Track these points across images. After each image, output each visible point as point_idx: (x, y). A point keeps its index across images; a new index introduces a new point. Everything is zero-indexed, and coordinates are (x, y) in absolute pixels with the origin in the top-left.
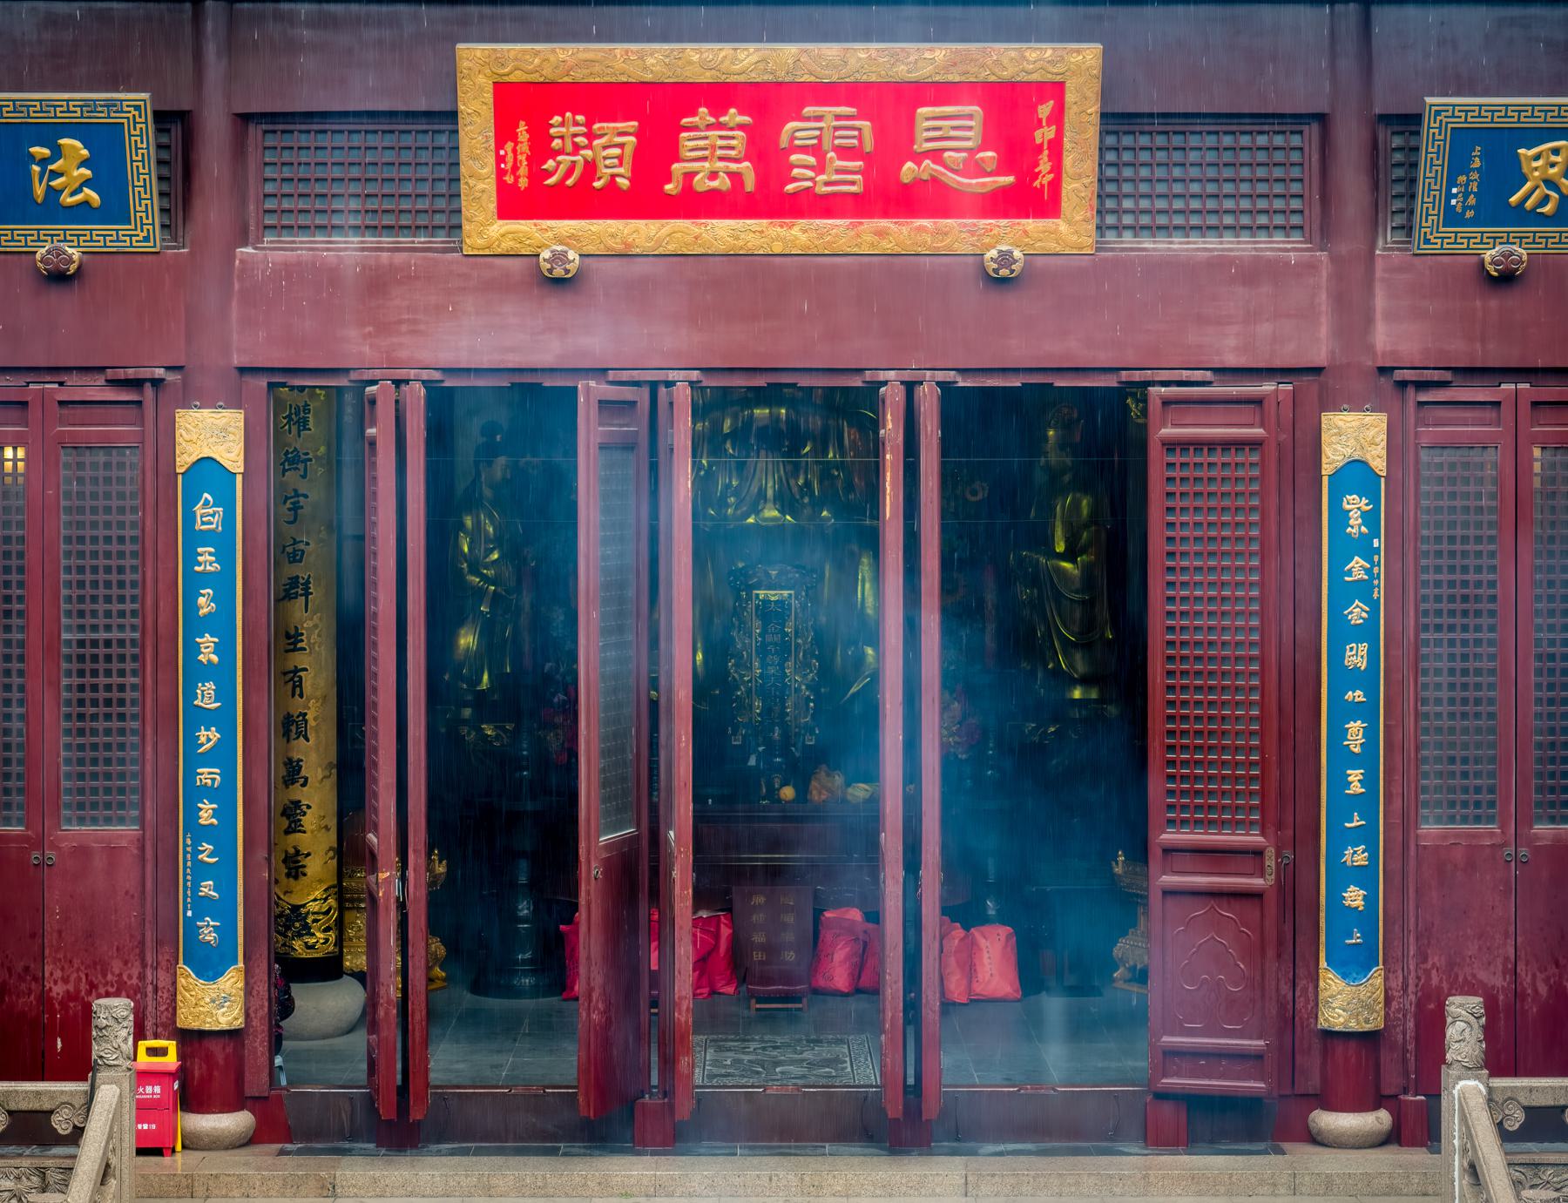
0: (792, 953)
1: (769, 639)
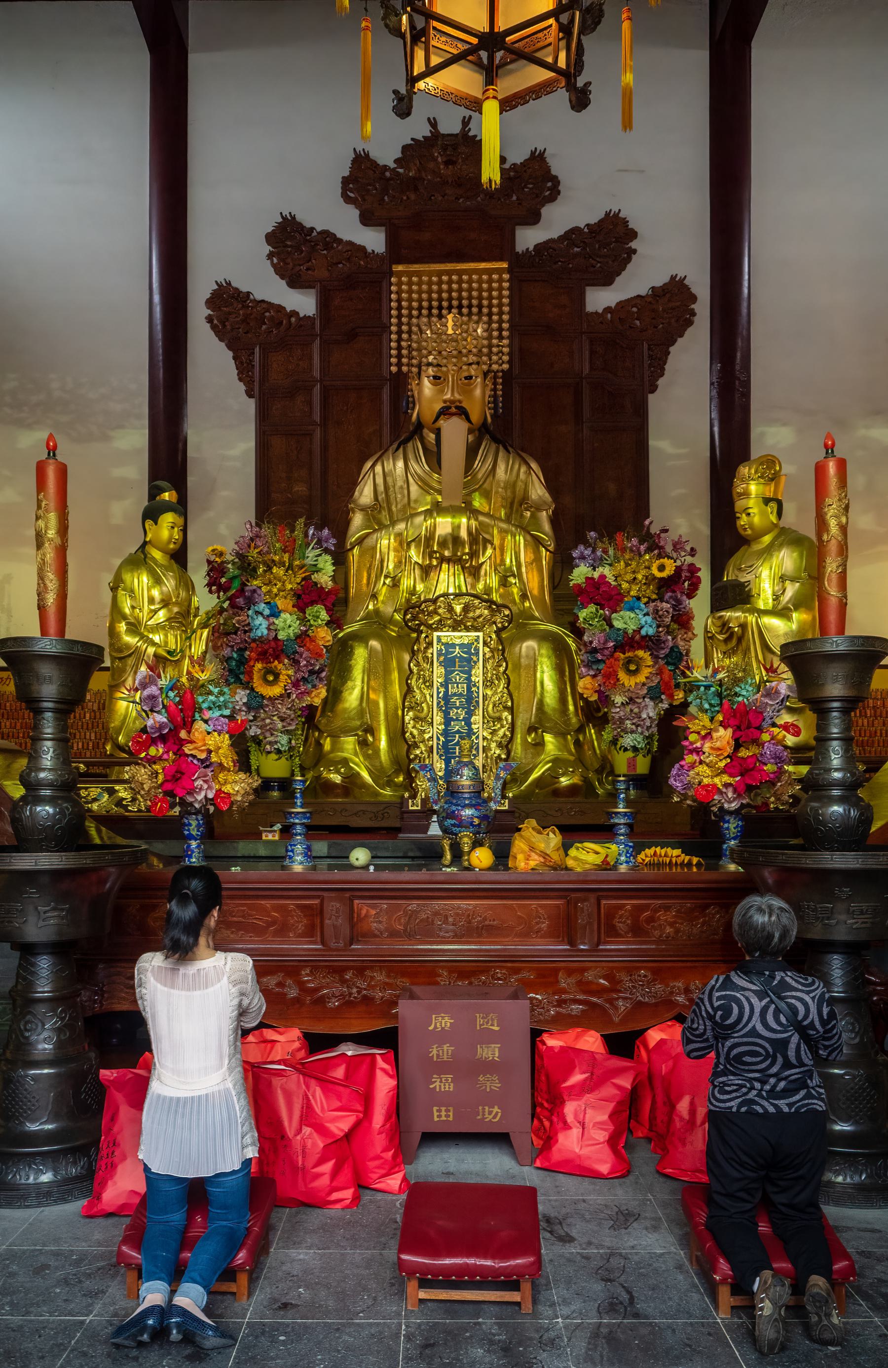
0: (496, 1109)
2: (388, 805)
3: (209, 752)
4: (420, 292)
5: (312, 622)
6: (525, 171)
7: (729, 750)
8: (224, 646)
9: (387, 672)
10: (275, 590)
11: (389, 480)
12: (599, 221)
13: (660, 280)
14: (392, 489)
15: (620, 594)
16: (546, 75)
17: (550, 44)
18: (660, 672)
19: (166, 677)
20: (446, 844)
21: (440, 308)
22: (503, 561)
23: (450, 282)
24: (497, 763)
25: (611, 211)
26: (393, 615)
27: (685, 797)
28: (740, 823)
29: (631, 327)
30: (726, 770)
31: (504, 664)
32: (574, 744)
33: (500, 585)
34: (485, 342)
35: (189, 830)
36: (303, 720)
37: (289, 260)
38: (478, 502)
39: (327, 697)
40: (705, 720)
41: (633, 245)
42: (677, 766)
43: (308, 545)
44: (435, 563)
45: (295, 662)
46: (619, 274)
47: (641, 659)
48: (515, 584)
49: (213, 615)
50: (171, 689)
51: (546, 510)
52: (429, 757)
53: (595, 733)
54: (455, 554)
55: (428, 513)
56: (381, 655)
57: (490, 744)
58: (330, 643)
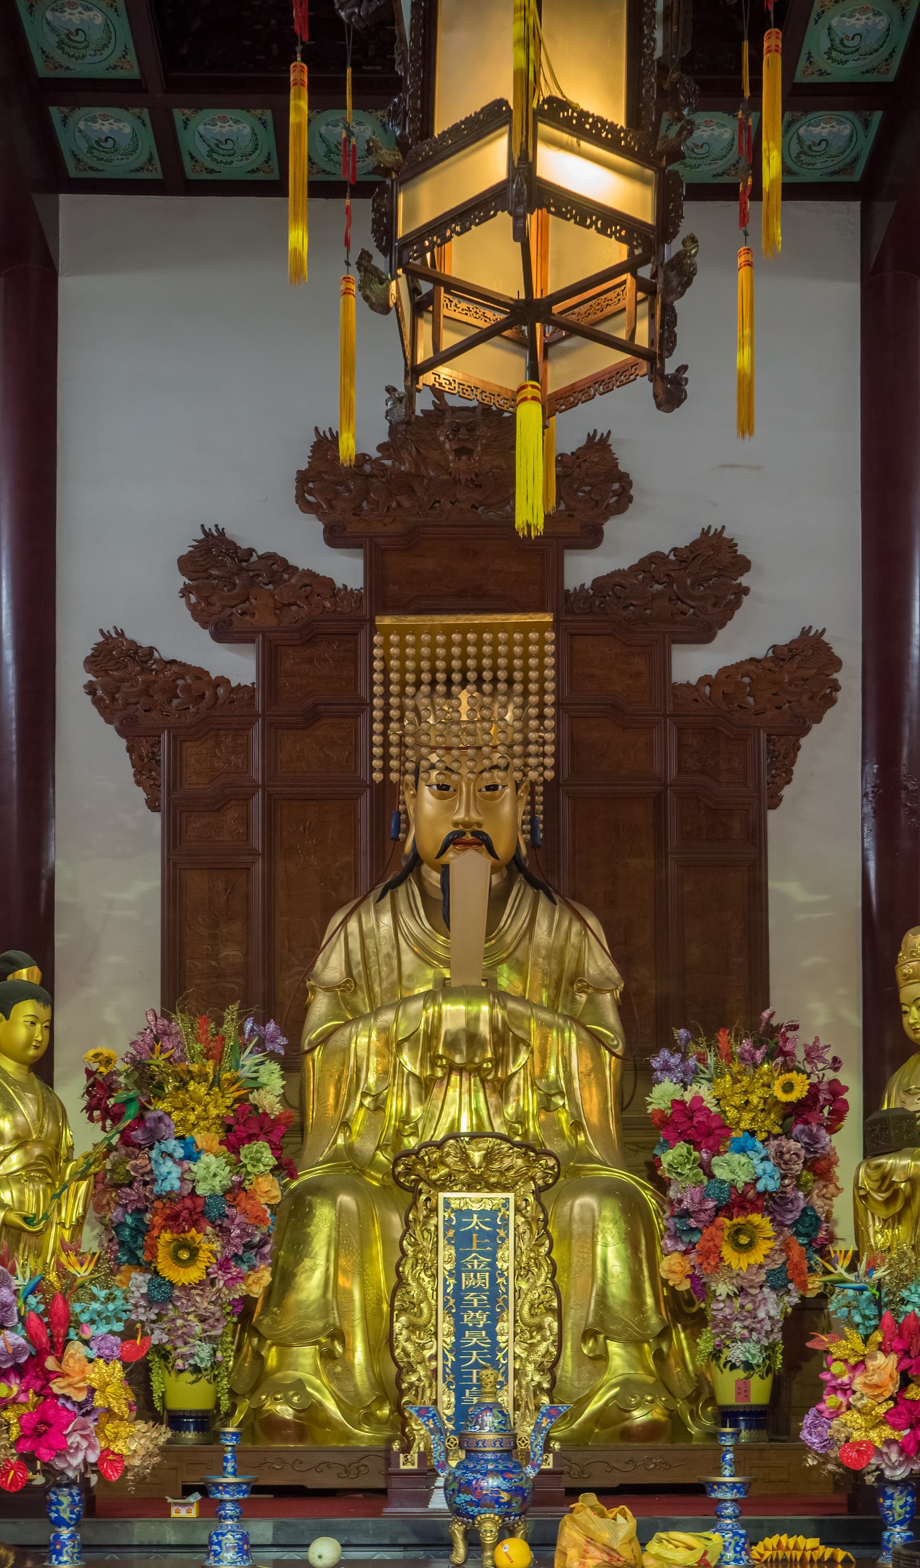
1: (467, 1281)
2: (367, 1453)
3: (92, 1391)
4: (418, 658)
5: (249, 1168)
6: (579, 466)
7: (892, 1388)
8: (112, 1205)
9: (365, 1242)
10: (192, 1118)
11: (370, 943)
13: (786, 635)
14: (373, 958)
15: (724, 1127)
16: (617, 357)
17: (624, 310)
18: (786, 1248)
19: (24, 1273)
20: (458, 1531)
21: (449, 682)
22: (544, 1071)
23: (464, 644)
24: (535, 1395)
26: (374, 1155)
27: (826, 1459)
28: (909, 1499)
29: (741, 707)
30: (889, 1419)
31: (547, 1242)
32: (654, 1356)
33: (539, 1109)
34: (518, 737)
35: (57, 1511)
36: (235, 1319)
37: (214, 599)
38: (506, 979)
39: (271, 1285)
40: (855, 1340)
41: (744, 580)
42: (813, 1411)
43: (243, 1047)
44: (439, 1073)
45: (224, 1231)
46: (722, 625)
47: (756, 1227)
48: (564, 1106)
49: (95, 1160)
50: (32, 1292)
51: (611, 991)
52: (430, 1386)
53: (686, 1337)
54: (470, 1060)
55: (430, 997)
56: (356, 1217)
57: (524, 1366)
58: (278, 1201)
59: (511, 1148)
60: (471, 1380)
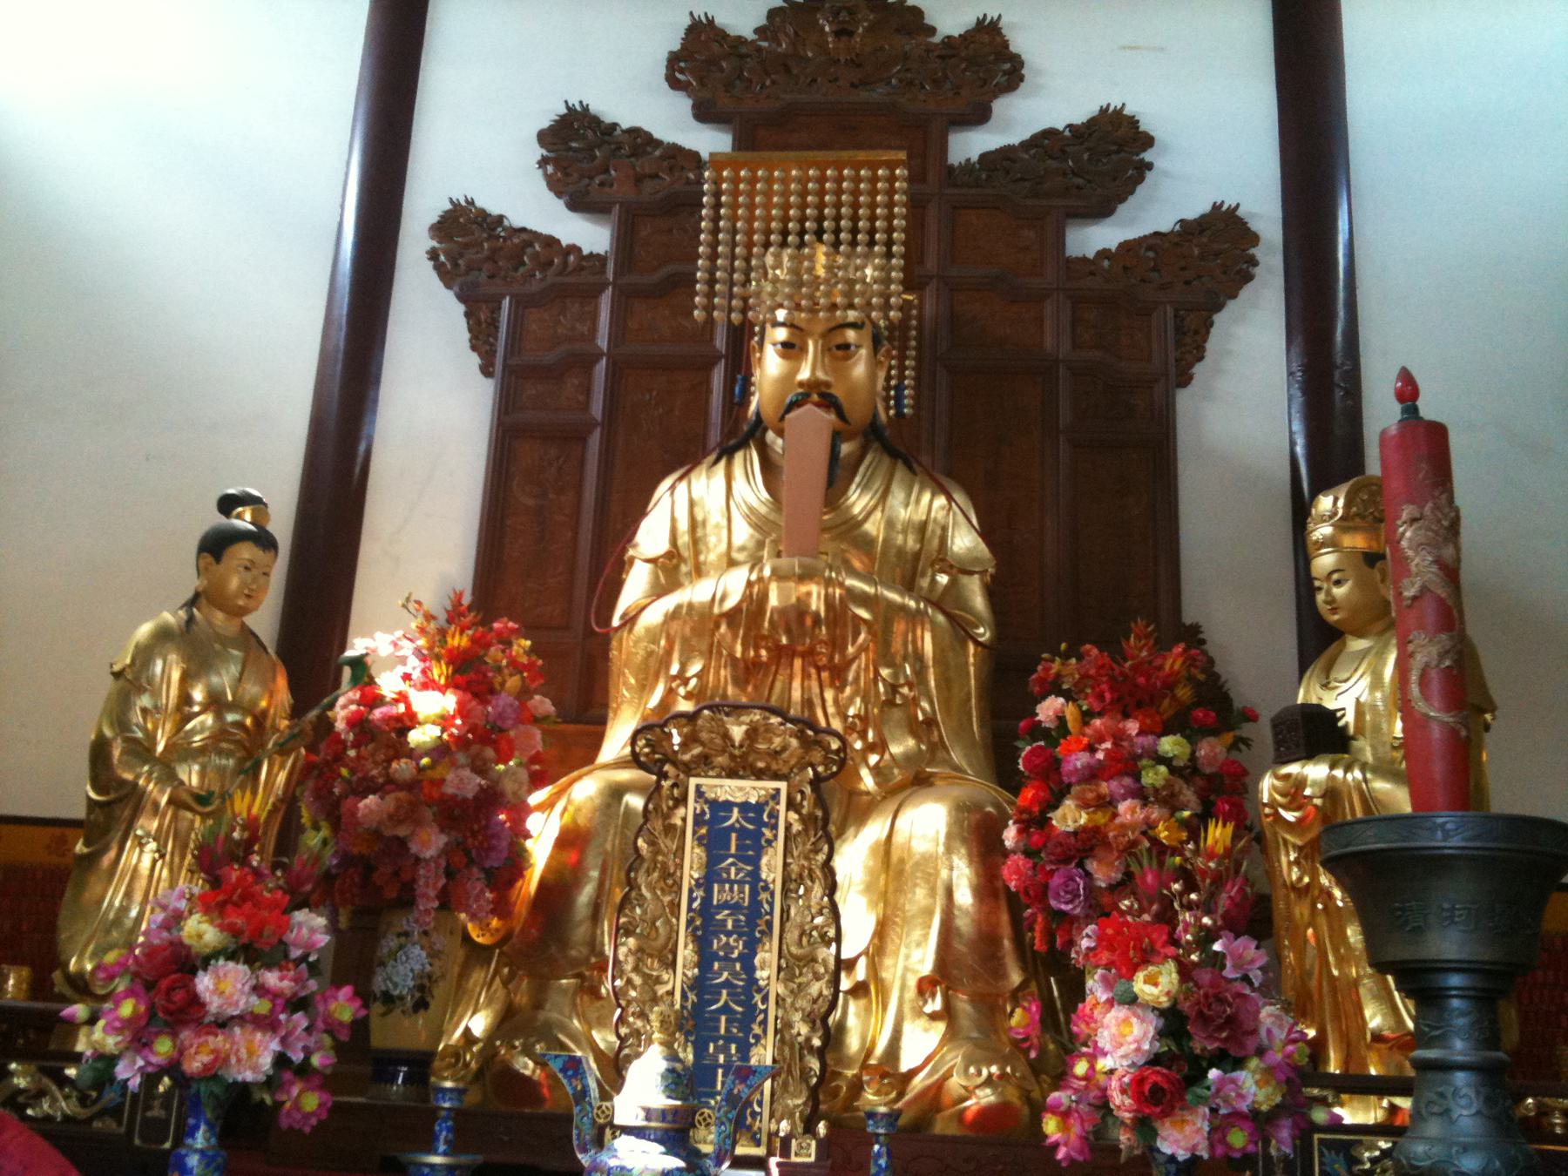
12: (1089, 121)
13: (1195, 208)
25: (1109, 105)
31: (826, 848)
41: (1148, 156)
59: (782, 724)
60: (717, 1029)
